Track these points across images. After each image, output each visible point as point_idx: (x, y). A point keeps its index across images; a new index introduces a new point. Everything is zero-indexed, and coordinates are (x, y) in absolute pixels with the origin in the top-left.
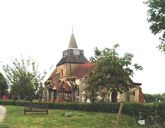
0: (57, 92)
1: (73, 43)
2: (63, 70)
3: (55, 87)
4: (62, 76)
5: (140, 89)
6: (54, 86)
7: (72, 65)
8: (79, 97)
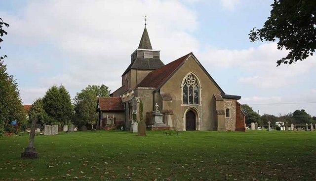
1: (145, 41)
7: (139, 72)
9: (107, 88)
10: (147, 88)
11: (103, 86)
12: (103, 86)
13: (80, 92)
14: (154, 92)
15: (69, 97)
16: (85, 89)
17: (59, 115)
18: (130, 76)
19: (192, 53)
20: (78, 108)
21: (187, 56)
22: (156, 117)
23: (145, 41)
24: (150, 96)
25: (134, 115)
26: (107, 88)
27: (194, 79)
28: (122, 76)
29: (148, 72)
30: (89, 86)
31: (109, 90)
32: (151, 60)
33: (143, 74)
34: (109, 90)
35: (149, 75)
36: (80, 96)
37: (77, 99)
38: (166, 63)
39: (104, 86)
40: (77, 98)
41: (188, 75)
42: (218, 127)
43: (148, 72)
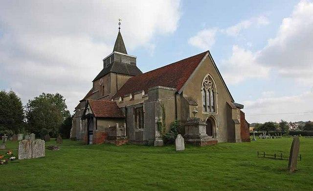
0: (94, 119)
1: (119, 44)
2: (103, 87)
3: (90, 109)
4: (103, 95)
5: (242, 114)
6: (89, 107)
7: (120, 77)
8: (142, 130)
9: (61, 97)
10: (169, 88)
11: (58, 95)
12: (58, 95)
13: (33, 99)
14: (177, 93)
15: (20, 103)
16: (38, 97)
17: (10, 123)
18: (109, 81)
19: (208, 51)
20: (30, 116)
21: (205, 53)
22: (200, 126)
23: (119, 44)
24: (172, 99)
25: (158, 123)
26: (61, 97)
27: (210, 83)
28: (94, 81)
29: (128, 78)
30: (43, 94)
31: (63, 99)
32: (128, 66)
33: (123, 79)
34: (63, 99)
35: (130, 80)
36: (33, 104)
37: (29, 107)
38: (144, 71)
39: (59, 94)
40: (29, 105)
41: (205, 78)
42: (236, 138)
43: (128, 78)
